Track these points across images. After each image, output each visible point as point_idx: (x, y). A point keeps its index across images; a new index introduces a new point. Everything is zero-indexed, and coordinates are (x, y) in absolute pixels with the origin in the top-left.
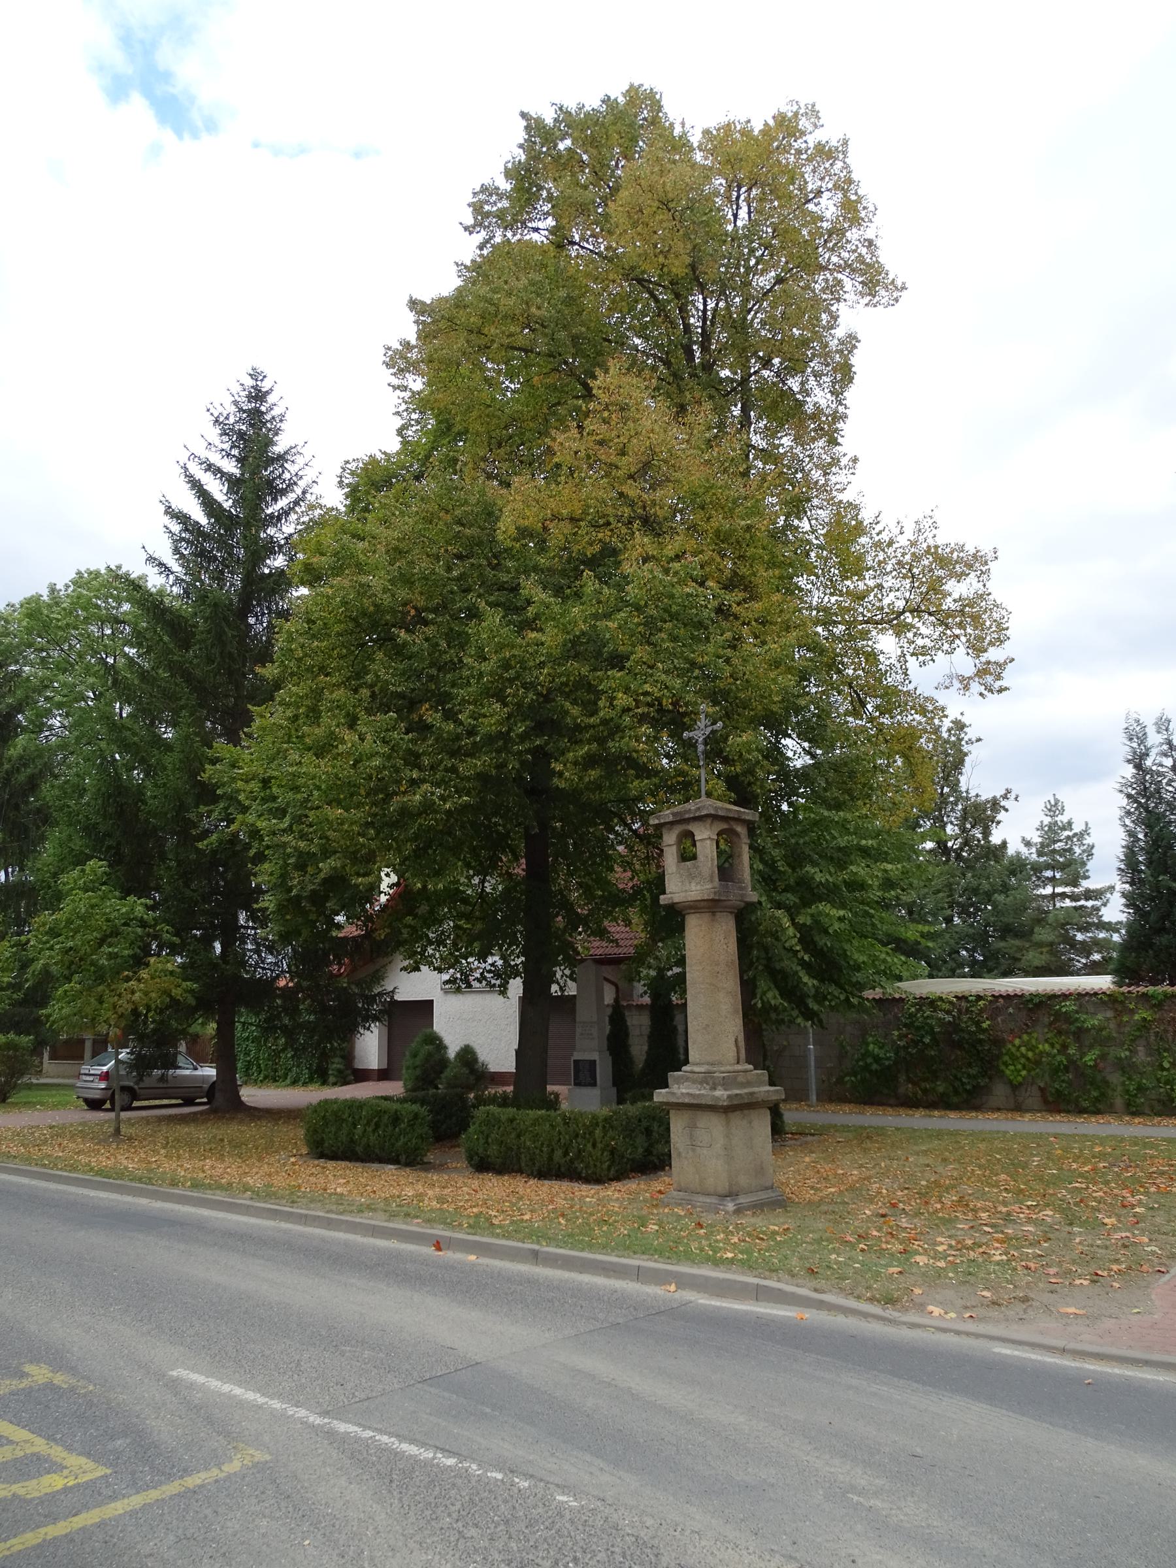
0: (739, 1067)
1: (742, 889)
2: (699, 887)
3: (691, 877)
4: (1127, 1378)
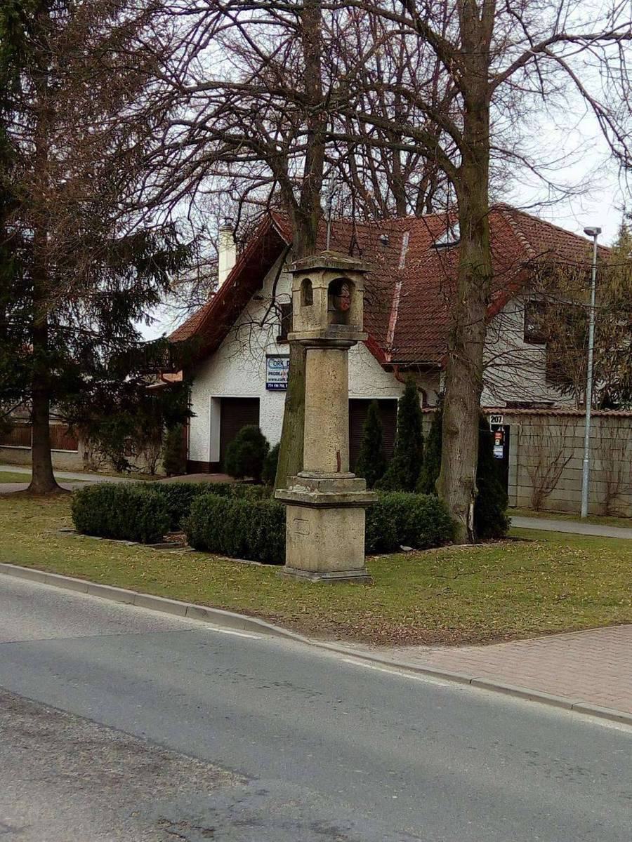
0: (338, 475)
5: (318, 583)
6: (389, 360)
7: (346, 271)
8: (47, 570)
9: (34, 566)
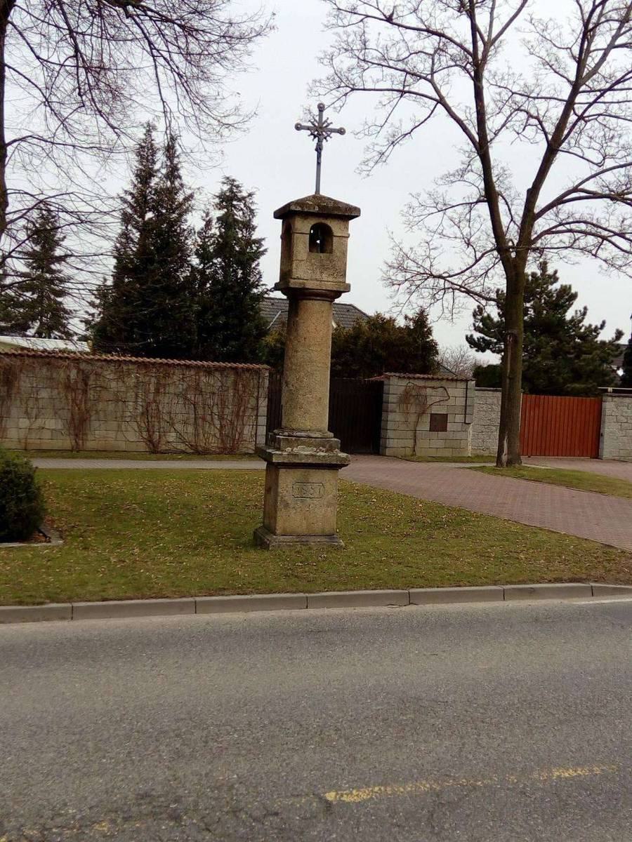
4: (614, 603)
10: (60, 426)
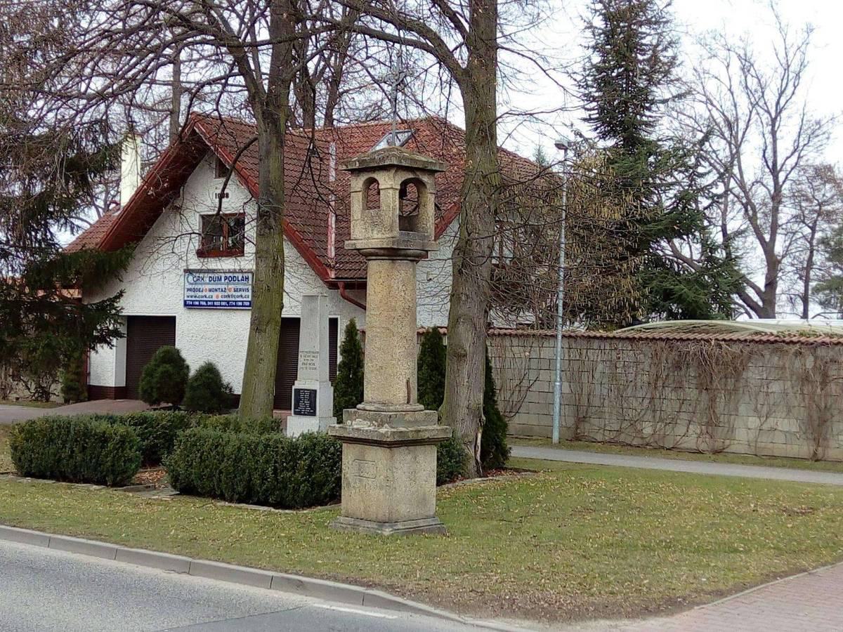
0: (409, 407)
1: (424, 238)
2: (380, 236)
3: (374, 224)
4: (352, 613)
5: (392, 535)
6: (333, 276)
7: (418, 169)
8: (132, 543)
9: (21, 525)
10: (794, 429)
